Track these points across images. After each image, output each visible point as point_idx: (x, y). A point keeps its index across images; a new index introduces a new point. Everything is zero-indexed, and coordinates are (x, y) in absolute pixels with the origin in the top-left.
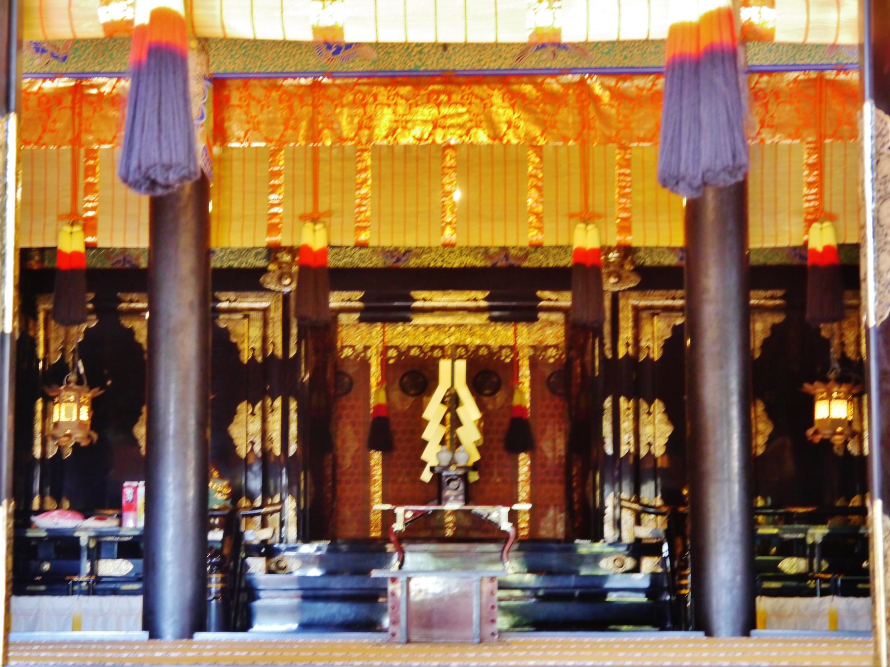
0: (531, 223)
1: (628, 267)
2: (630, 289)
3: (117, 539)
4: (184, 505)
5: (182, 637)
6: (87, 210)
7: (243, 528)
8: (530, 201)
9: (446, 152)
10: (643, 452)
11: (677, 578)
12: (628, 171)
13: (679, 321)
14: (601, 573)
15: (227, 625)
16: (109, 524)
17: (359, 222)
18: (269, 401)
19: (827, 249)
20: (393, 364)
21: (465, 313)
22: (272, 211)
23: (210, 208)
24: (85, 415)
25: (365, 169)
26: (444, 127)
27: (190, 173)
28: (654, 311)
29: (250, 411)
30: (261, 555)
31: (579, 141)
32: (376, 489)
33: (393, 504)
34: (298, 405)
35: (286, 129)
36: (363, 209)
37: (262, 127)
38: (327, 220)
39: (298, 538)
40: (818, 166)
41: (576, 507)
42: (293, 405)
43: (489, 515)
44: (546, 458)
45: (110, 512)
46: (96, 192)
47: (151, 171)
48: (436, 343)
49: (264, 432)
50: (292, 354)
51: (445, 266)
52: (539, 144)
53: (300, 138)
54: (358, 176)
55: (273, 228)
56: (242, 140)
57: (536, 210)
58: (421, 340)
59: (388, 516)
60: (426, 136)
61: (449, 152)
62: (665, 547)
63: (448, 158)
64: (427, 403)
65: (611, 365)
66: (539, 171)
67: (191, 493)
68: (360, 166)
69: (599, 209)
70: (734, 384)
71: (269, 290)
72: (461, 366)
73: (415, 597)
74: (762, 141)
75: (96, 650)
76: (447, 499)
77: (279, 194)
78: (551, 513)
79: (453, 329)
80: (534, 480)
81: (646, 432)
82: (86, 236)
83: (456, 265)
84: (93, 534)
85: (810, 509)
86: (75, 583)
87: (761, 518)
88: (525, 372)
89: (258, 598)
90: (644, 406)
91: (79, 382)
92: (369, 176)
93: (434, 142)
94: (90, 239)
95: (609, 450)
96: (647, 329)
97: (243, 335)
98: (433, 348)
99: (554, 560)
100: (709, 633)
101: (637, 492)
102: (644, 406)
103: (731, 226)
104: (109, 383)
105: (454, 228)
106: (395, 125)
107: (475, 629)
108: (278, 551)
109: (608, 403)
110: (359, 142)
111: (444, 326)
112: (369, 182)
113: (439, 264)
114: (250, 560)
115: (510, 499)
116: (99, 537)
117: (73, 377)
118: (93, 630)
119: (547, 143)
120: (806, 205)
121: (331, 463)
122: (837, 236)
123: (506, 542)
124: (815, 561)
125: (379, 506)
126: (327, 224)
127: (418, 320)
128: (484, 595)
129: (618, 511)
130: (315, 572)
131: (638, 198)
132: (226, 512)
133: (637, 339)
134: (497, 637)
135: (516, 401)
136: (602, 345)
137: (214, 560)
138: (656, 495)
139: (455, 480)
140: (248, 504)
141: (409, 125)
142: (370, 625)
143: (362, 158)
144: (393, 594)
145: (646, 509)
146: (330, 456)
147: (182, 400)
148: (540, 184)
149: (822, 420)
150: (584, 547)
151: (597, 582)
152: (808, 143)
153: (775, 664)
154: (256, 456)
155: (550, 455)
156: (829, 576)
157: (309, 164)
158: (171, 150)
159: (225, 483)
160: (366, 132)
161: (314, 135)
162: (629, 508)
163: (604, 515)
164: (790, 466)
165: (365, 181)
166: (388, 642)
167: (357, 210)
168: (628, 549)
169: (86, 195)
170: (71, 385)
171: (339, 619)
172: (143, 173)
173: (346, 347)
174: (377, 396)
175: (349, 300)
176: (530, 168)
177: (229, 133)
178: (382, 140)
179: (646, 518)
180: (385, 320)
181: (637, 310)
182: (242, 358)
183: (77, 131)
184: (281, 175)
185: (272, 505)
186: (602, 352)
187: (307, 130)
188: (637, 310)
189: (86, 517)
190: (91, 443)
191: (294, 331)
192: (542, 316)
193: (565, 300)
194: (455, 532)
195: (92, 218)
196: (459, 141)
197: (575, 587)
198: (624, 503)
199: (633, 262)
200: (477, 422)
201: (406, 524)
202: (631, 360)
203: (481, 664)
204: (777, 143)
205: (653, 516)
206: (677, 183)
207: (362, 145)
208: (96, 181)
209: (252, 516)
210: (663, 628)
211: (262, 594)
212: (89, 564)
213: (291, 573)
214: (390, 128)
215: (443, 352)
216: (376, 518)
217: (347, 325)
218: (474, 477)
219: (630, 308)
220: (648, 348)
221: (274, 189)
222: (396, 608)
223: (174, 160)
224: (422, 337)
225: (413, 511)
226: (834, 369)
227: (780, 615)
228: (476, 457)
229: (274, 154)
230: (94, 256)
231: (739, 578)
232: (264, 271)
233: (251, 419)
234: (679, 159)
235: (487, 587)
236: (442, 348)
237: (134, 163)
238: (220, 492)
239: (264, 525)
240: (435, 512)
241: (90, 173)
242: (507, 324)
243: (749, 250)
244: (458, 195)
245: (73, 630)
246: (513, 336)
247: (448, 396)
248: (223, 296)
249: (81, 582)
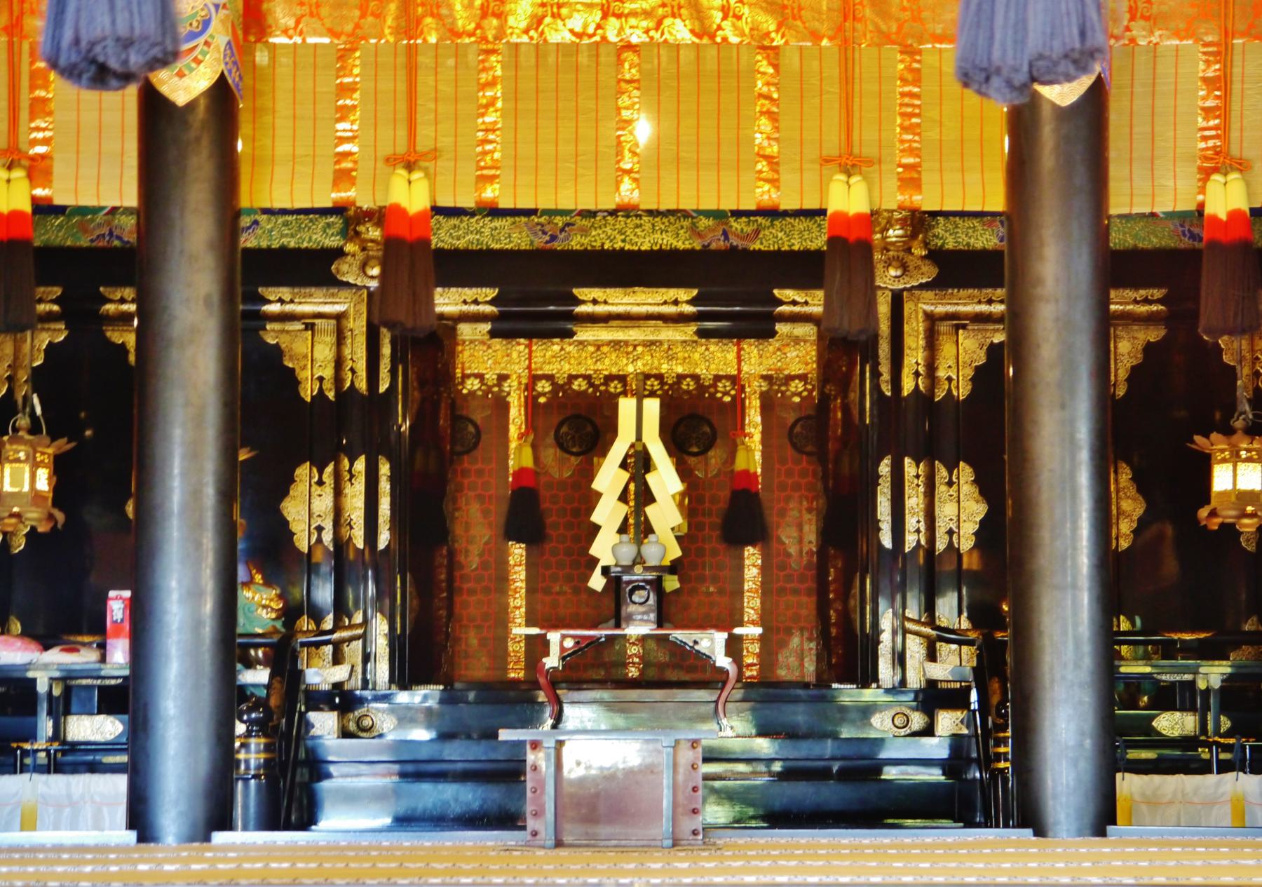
0: (760, 172)
1: (919, 251)
2: (922, 287)
3: (99, 682)
4: (197, 625)
5: (192, 839)
6: (34, 142)
7: (302, 664)
8: (759, 138)
9: (625, 55)
10: (941, 545)
11: (992, 743)
12: (916, 90)
13: (999, 338)
14: (873, 735)
15: (273, 819)
16: (84, 658)
17: (483, 168)
18: (346, 463)
19: (1235, 215)
20: (545, 404)
21: (660, 323)
22: (340, 149)
23: (240, 146)
24: (43, 482)
25: (492, 84)
26: (619, 16)
27: (165, 52)
28: (959, 322)
29: (316, 479)
30: (333, 708)
31: (838, 41)
32: (518, 603)
33: (542, 628)
34: (391, 468)
35: (363, 16)
36: (488, 147)
37: (324, 11)
38: (430, 165)
39: (391, 680)
40: (1221, 83)
41: (834, 631)
42: (385, 469)
43: (696, 642)
44: (789, 555)
45: (86, 639)
46: (50, 114)
47: (98, 49)
48: (614, 370)
49: (338, 511)
50: (383, 387)
51: (627, 247)
52: (775, 44)
53: (387, 31)
54: (481, 94)
55: (343, 177)
56: (291, 32)
57: (768, 151)
58: (588, 367)
59: (537, 646)
60: (590, 30)
61: (629, 56)
62: (974, 696)
63: (627, 65)
64: (600, 465)
65: (890, 406)
66: (773, 89)
67: (208, 606)
68: (484, 77)
69: (869, 151)
70: (1083, 432)
71: (347, 285)
72: (652, 407)
73: (571, 771)
74: (1133, 40)
75: (46, 861)
76: (630, 618)
77: (353, 123)
78: (795, 641)
79: (640, 349)
80: (766, 590)
81: (946, 512)
82: (33, 186)
83: (645, 247)
84: (57, 674)
85: (1202, 636)
86: (25, 753)
87: (1124, 650)
88: (754, 416)
89: (328, 776)
90: (942, 472)
91: (34, 429)
92: (499, 94)
93: (604, 38)
94: (39, 192)
95: (887, 541)
96: (947, 350)
97: (305, 357)
98: (609, 378)
99: (799, 715)
100: (1040, 831)
101: (930, 608)
102: (942, 472)
103: (1081, 177)
104: (88, 433)
105: (635, 180)
106: (540, 11)
107: (666, 825)
108: (361, 701)
109: (885, 468)
110: (484, 39)
111: (626, 343)
112: (499, 104)
113: (618, 245)
114: (312, 716)
115: (727, 619)
116: (67, 679)
117: (23, 421)
118: (56, 827)
119: (786, 43)
120: (1202, 145)
121: (445, 562)
122: (1250, 195)
123: (722, 689)
124: (1210, 717)
125: (520, 630)
126: (432, 171)
127: (586, 334)
128: (681, 770)
129: (899, 639)
130: (422, 734)
131: (932, 134)
132: (275, 639)
133: (931, 367)
134: (700, 837)
135: (740, 464)
136: (876, 375)
137: (253, 715)
138: (960, 613)
139: (643, 588)
140: (312, 626)
141: (564, 11)
142: (508, 819)
143: (487, 64)
144: (535, 768)
145: (947, 635)
146: (444, 552)
147: (193, 455)
148: (775, 109)
149: (1224, 494)
150: (848, 694)
151: (865, 750)
152: (1206, 45)
153: (1146, 881)
154: (326, 548)
155: (793, 550)
156: (1232, 741)
157: (402, 75)
158: (131, 13)
159: (273, 593)
160: (495, 22)
161: (409, 27)
162: (916, 633)
163: (878, 642)
164: (1171, 566)
165: (492, 102)
166: (528, 845)
167: (479, 149)
168: (915, 699)
169: (32, 118)
170: (21, 433)
171: (456, 809)
172: (84, 51)
173: (469, 376)
174: (519, 456)
175: (476, 302)
176: (759, 84)
177: (270, 21)
178: (519, 36)
179: (943, 649)
180: (530, 335)
181: (932, 320)
182: (302, 394)
183: (16, 13)
184: (354, 90)
185: (351, 627)
186: (876, 388)
187: (397, 18)
188: (932, 320)
189: (46, 648)
190: (54, 528)
191: (386, 350)
192: (782, 328)
193: (815, 302)
194: (642, 672)
195: (43, 157)
196: (645, 38)
197: (833, 759)
198: (909, 625)
199: (926, 244)
200: (678, 497)
201: (563, 659)
202: (923, 399)
203: (700, 880)
204: (1156, 44)
205: (954, 647)
206: (987, 79)
207: (487, 42)
208: (50, 96)
209: (318, 645)
210: (970, 824)
211: (332, 769)
212: (50, 724)
213: (381, 736)
214: (533, 16)
215: (625, 385)
216: (516, 649)
217: (472, 342)
218: (671, 583)
219: (921, 315)
220: (949, 379)
221: (344, 113)
222: (538, 792)
223: (137, 32)
224: (590, 361)
225: (573, 637)
226: (1245, 413)
227: (1154, 802)
228: (675, 552)
229: (343, 55)
230: (60, 226)
231: (1088, 743)
232: (339, 253)
233: (316, 490)
234: (992, 37)
235: (687, 756)
236: (622, 379)
237: (68, 35)
238: (265, 607)
239: (337, 659)
240: (611, 639)
241: (40, 82)
242: (725, 341)
243: (1109, 217)
244: (643, 130)
245: (22, 829)
246: (735, 361)
247: (630, 456)
248: (271, 293)
249: (37, 751)
